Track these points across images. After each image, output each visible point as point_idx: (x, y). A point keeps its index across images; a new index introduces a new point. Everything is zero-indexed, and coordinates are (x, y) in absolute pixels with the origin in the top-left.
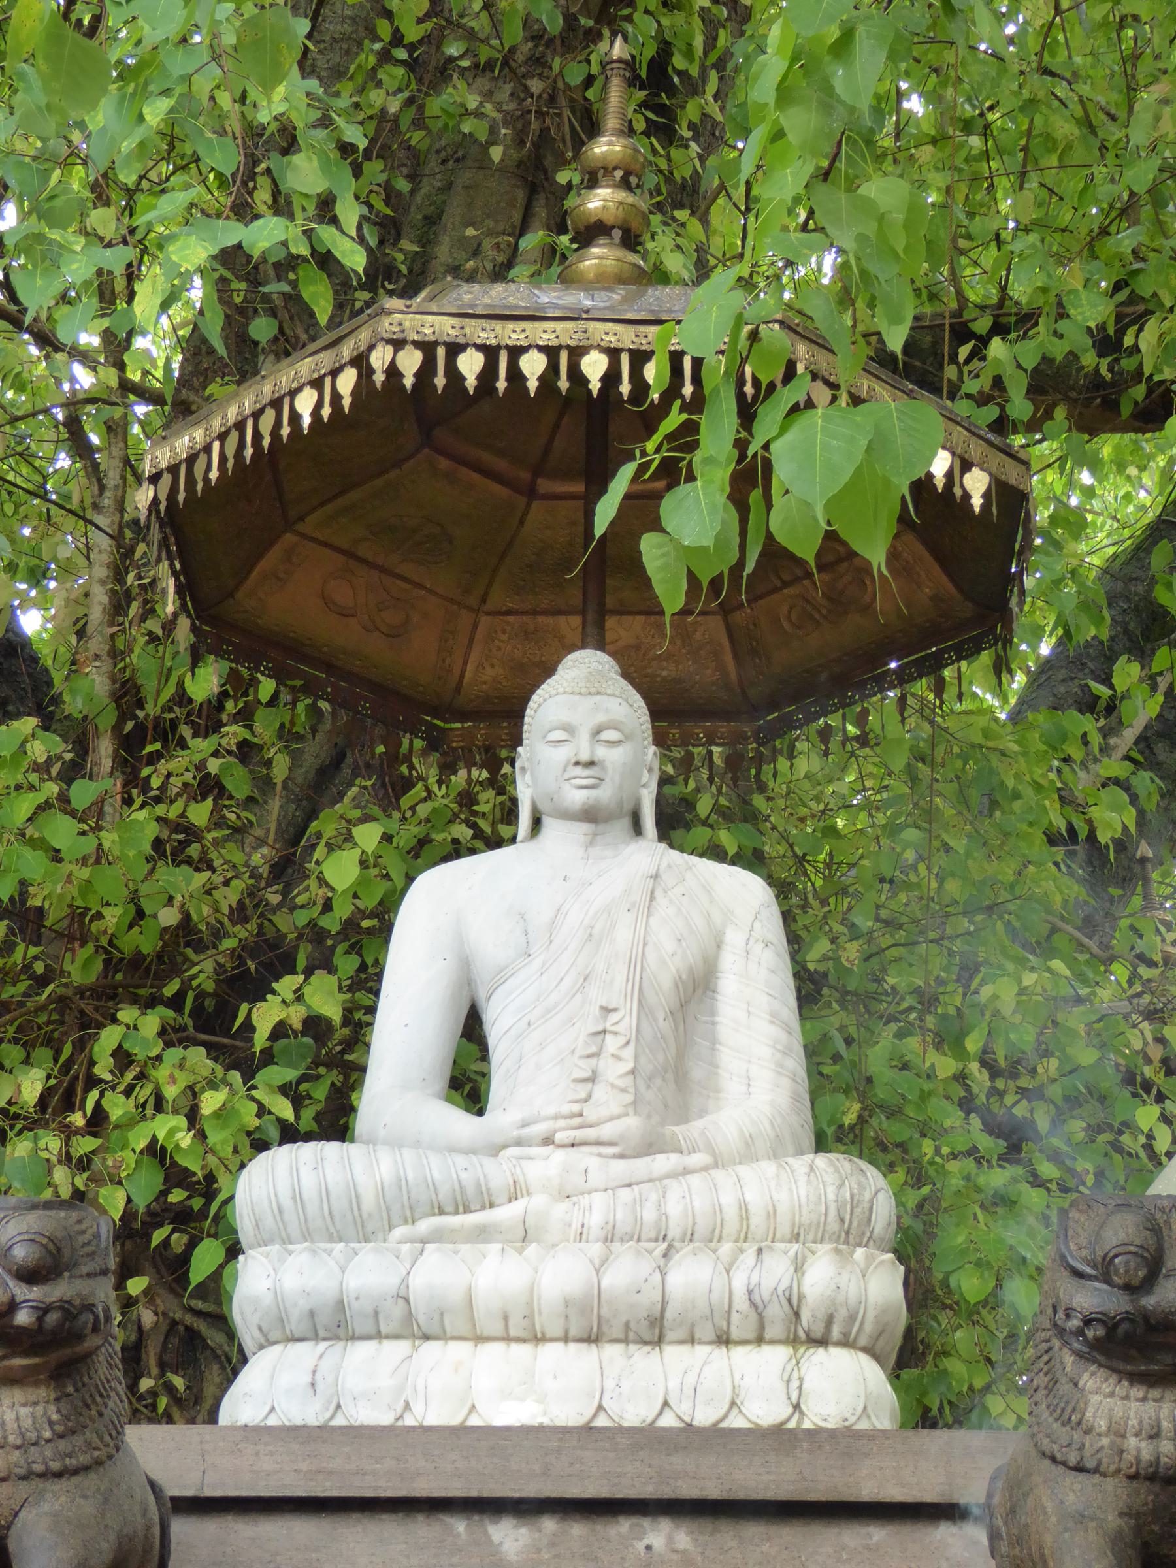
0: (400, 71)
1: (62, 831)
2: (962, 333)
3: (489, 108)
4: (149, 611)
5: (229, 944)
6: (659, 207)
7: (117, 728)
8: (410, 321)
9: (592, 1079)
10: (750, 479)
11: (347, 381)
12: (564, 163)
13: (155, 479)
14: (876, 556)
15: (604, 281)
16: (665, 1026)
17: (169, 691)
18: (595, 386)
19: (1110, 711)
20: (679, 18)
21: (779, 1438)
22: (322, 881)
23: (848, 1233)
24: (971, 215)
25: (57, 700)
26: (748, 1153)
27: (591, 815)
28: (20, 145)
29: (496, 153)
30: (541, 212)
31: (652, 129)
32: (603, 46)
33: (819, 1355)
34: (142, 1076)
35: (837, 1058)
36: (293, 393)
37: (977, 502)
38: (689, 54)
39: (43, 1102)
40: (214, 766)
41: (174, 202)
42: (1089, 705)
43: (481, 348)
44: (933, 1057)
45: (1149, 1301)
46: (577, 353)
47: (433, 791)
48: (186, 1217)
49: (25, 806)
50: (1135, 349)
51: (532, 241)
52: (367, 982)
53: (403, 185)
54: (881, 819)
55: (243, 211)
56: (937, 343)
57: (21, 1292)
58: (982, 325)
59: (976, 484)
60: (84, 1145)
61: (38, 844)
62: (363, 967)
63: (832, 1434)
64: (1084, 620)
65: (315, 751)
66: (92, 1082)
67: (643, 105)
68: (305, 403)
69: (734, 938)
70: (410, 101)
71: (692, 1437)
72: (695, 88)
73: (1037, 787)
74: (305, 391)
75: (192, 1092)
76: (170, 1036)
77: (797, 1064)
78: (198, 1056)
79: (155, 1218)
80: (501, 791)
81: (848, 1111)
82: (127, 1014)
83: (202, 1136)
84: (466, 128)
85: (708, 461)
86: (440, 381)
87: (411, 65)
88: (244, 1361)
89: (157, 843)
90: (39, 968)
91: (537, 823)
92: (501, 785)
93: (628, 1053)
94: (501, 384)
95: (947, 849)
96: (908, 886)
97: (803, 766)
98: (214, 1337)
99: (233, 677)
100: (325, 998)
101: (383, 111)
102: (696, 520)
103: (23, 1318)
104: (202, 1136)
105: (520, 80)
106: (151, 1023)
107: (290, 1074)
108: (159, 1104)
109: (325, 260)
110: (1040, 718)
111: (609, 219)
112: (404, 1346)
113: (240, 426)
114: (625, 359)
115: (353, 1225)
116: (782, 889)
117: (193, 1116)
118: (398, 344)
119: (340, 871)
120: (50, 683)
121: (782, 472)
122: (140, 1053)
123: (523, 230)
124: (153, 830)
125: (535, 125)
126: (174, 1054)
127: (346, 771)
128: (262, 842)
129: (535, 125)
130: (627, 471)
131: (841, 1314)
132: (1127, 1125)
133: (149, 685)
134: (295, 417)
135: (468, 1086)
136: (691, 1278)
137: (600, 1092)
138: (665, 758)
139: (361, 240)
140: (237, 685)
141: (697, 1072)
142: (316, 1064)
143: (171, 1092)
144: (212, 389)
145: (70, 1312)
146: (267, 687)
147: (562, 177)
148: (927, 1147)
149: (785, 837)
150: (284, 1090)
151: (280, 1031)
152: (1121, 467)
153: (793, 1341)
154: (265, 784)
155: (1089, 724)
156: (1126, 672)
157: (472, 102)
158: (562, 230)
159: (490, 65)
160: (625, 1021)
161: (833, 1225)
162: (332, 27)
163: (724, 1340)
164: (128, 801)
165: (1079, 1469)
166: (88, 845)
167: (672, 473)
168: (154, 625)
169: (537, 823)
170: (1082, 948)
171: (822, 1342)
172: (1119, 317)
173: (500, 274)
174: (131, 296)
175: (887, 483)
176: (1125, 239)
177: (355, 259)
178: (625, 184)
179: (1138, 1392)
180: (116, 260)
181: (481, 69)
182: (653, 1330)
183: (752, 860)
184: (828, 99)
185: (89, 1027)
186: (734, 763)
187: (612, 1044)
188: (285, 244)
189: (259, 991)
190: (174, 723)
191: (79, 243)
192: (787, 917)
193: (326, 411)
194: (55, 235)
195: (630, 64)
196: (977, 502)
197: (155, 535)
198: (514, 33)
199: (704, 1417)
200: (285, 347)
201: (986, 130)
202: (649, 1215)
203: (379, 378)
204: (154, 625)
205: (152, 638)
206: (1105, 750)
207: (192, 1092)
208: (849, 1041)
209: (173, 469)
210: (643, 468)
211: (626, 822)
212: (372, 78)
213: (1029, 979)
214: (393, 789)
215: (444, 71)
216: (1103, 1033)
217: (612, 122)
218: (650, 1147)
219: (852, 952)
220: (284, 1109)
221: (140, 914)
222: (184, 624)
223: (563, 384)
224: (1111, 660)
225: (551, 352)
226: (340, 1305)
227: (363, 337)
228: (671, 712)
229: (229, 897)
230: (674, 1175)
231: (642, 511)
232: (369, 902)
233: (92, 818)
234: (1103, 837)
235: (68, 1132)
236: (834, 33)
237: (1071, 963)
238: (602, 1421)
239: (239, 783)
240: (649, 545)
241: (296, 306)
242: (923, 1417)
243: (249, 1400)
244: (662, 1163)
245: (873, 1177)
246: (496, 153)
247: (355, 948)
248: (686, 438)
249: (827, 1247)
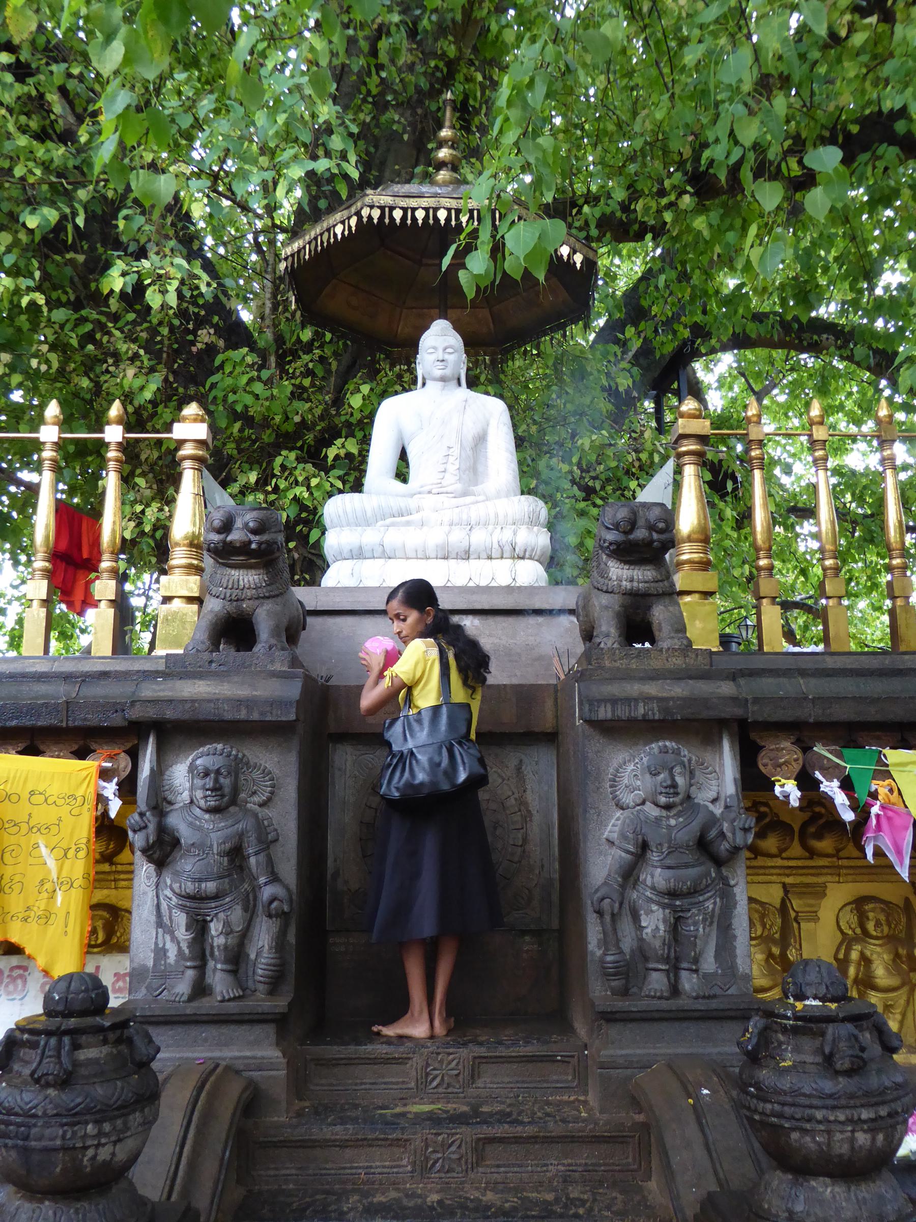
0: (370, 106)
1: (258, 388)
2: (574, 204)
3: (402, 120)
4: (286, 310)
5: (318, 428)
6: (465, 157)
7: (277, 352)
8: (375, 198)
9: (444, 472)
10: (498, 250)
11: (353, 221)
12: (429, 141)
13: (286, 259)
14: (541, 276)
15: (445, 184)
16: (470, 453)
17: (294, 339)
18: (442, 222)
19: (624, 344)
20: (471, 85)
21: (509, 589)
22: (350, 406)
23: (532, 522)
24: (677, 794)
25: (255, 342)
26: (498, 496)
27: (443, 379)
28: (232, 134)
29: (406, 137)
30: (422, 159)
31: (462, 128)
32: (444, 96)
33: (521, 562)
34: (291, 474)
35: (528, 466)
36: (334, 226)
37: (578, 266)
38: (475, 99)
39: (257, 482)
40: (311, 365)
41: (289, 153)
42: (617, 342)
43: (401, 208)
44: (561, 465)
45: (631, 537)
46: (436, 210)
47: (388, 373)
48: (309, 519)
49: (244, 379)
50: (635, 210)
51: (419, 170)
52: (366, 441)
53: (372, 150)
54: (544, 383)
55: (314, 158)
56: (565, 208)
57: (252, 537)
58: (581, 202)
59: (578, 258)
60: (272, 497)
61: (251, 393)
62: (365, 436)
63: (526, 587)
64: (616, 311)
65: (346, 359)
66: (274, 476)
67: (459, 118)
68: (339, 229)
69: (493, 423)
70: (373, 118)
71: (479, 590)
72: (477, 112)
73: (599, 371)
74: (339, 225)
75: (307, 479)
76: (299, 460)
77: (514, 466)
78: (309, 466)
79: (297, 523)
80: (412, 373)
81: (530, 480)
82: (284, 453)
83: (311, 494)
84: (395, 128)
85: (483, 243)
86: (387, 221)
87: (374, 103)
88: (328, 566)
89: (292, 393)
90: (253, 437)
91: (424, 384)
92: (412, 371)
93: (457, 462)
94: (409, 222)
95: (567, 393)
96: (553, 406)
97: (517, 363)
98: (319, 562)
99: (316, 333)
100: (352, 447)
101: (364, 121)
102: (479, 262)
103: (254, 546)
104: (311, 494)
105: (414, 109)
106: (292, 455)
107: (341, 473)
108: (297, 483)
109: (346, 177)
110: (600, 347)
111: (447, 160)
112: (382, 561)
113: (316, 239)
114: (453, 212)
115: (364, 521)
116: (510, 408)
117: (309, 488)
118: (372, 207)
119: (356, 401)
120: (252, 336)
121: (509, 244)
122: (289, 465)
123: (416, 165)
124: (290, 388)
125: (419, 126)
126: (301, 466)
127: (357, 366)
128: (328, 393)
129: (419, 126)
130: (453, 248)
131: (529, 549)
132: (627, 488)
133: (287, 336)
134: (335, 235)
135: (402, 475)
136: (479, 538)
137: (447, 475)
138: (469, 361)
139: (357, 168)
140: (318, 336)
141: (480, 468)
142: (350, 469)
143: (300, 479)
144: (305, 227)
145: (270, 544)
146: (328, 336)
147: (430, 146)
148: (559, 495)
149: (511, 389)
150: (339, 478)
151: (337, 457)
152: (629, 257)
153: (513, 558)
154: (328, 372)
155: (616, 349)
156: (630, 331)
157: (396, 118)
158: (430, 165)
159: (402, 103)
160: (456, 451)
161: (527, 519)
162: (345, 89)
163: (490, 558)
164: (281, 378)
165: (607, 592)
166: (268, 393)
167: (469, 248)
168: (288, 315)
169: (424, 384)
170: (613, 427)
171: (523, 558)
172: (629, 199)
173: (408, 181)
174: (275, 190)
175: (545, 249)
176: (632, 168)
177: (355, 174)
178: (452, 147)
179: (627, 567)
180: (269, 175)
181: (399, 105)
182: (466, 555)
183: (501, 397)
184: (525, 105)
185: (272, 457)
186: (493, 361)
187: (451, 459)
188: (329, 169)
189: (330, 444)
190: (296, 350)
191: (255, 170)
192: (512, 417)
193: (346, 233)
194: (247, 167)
195: (453, 101)
196: (578, 266)
197: (287, 280)
198: (411, 90)
199: (483, 583)
200: (331, 210)
201: (583, 129)
202: (465, 517)
203: (365, 220)
204: (288, 315)
205: (287, 319)
206: (622, 359)
207: (307, 479)
208: (533, 460)
209: (292, 255)
210: (459, 246)
211: (456, 381)
212: (359, 109)
213: (594, 437)
214: (373, 374)
215: (386, 106)
216: (618, 457)
217: (447, 123)
218: (465, 494)
219: (534, 428)
220: (339, 485)
221: (287, 418)
222: (299, 313)
223: (431, 222)
224: (625, 327)
225: (426, 209)
226: (361, 548)
227: (359, 204)
228: (472, 344)
229: (318, 411)
230: (473, 503)
231: (459, 262)
232: (367, 413)
233: (269, 383)
234: (621, 389)
235: (267, 493)
236: (527, 79)
237: (609, 432)
238: (449, 584)
239: (320, 372)
240: (462, 274)
241: (335, 194)
242: (555, 582)
243: (330, 579)
244: (469, 499)
245: (541, 503)
246: (406, 137)
247: (362, 429)
248: (474, 234)
249: (525, 526)
